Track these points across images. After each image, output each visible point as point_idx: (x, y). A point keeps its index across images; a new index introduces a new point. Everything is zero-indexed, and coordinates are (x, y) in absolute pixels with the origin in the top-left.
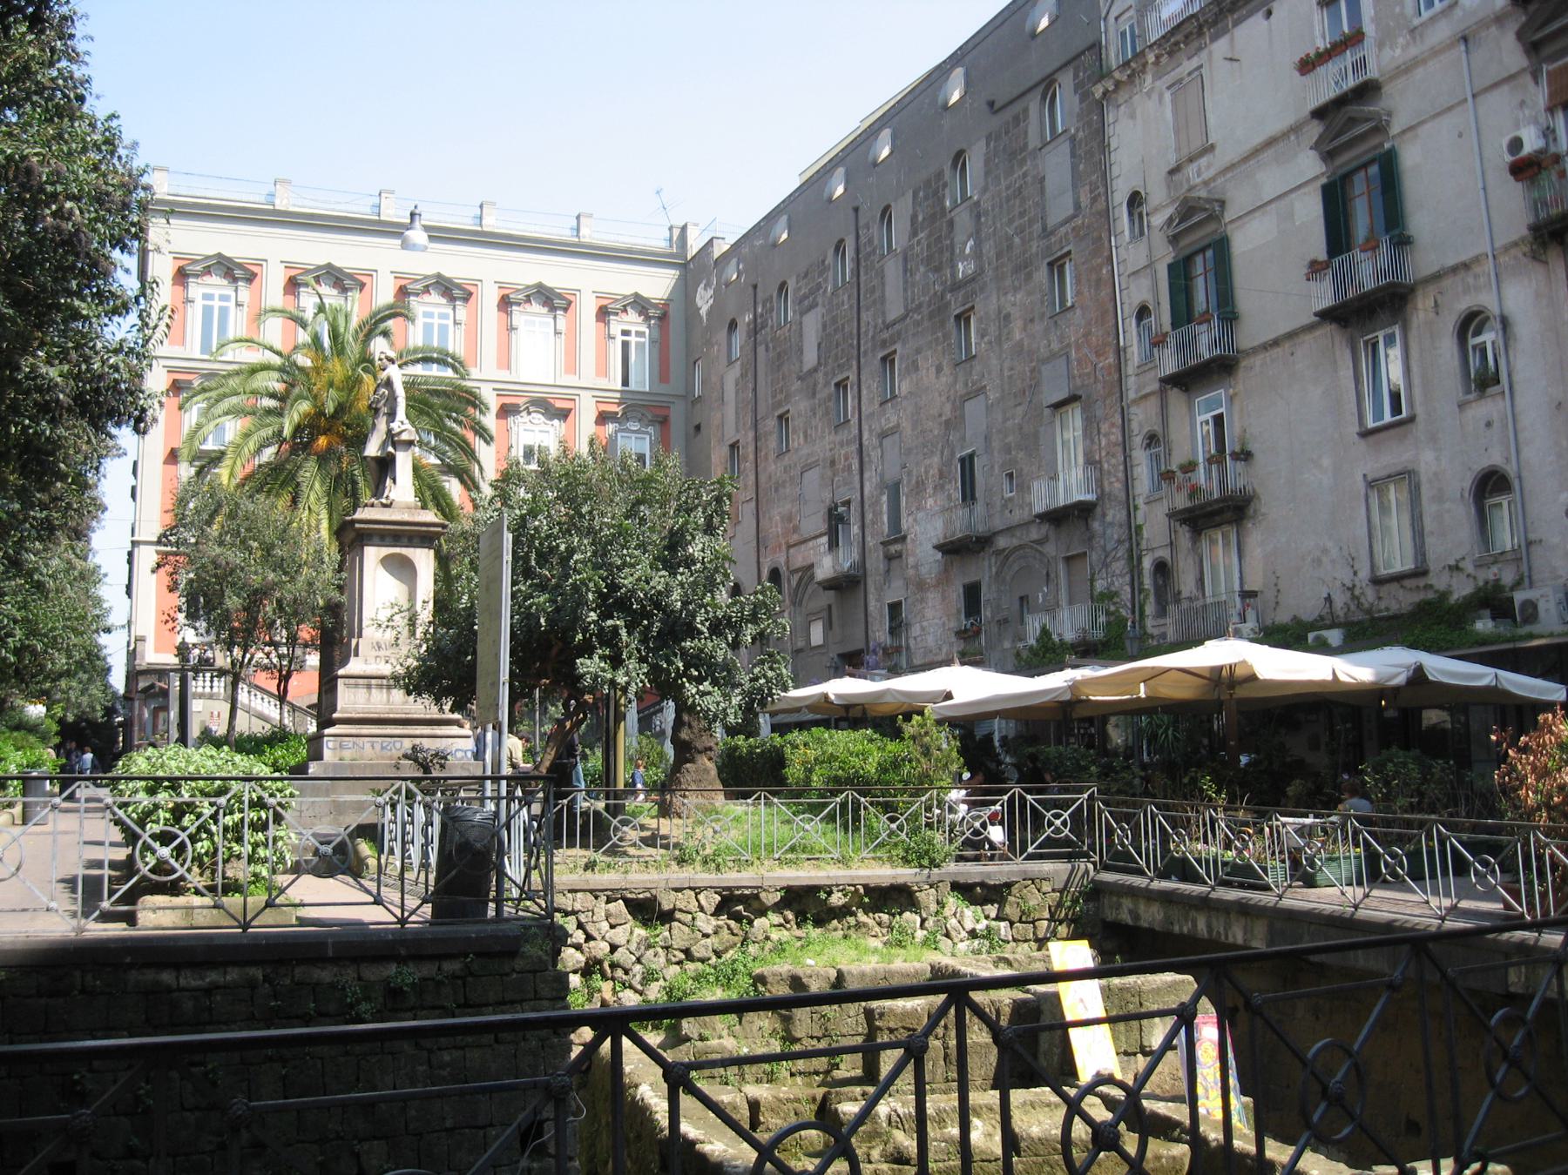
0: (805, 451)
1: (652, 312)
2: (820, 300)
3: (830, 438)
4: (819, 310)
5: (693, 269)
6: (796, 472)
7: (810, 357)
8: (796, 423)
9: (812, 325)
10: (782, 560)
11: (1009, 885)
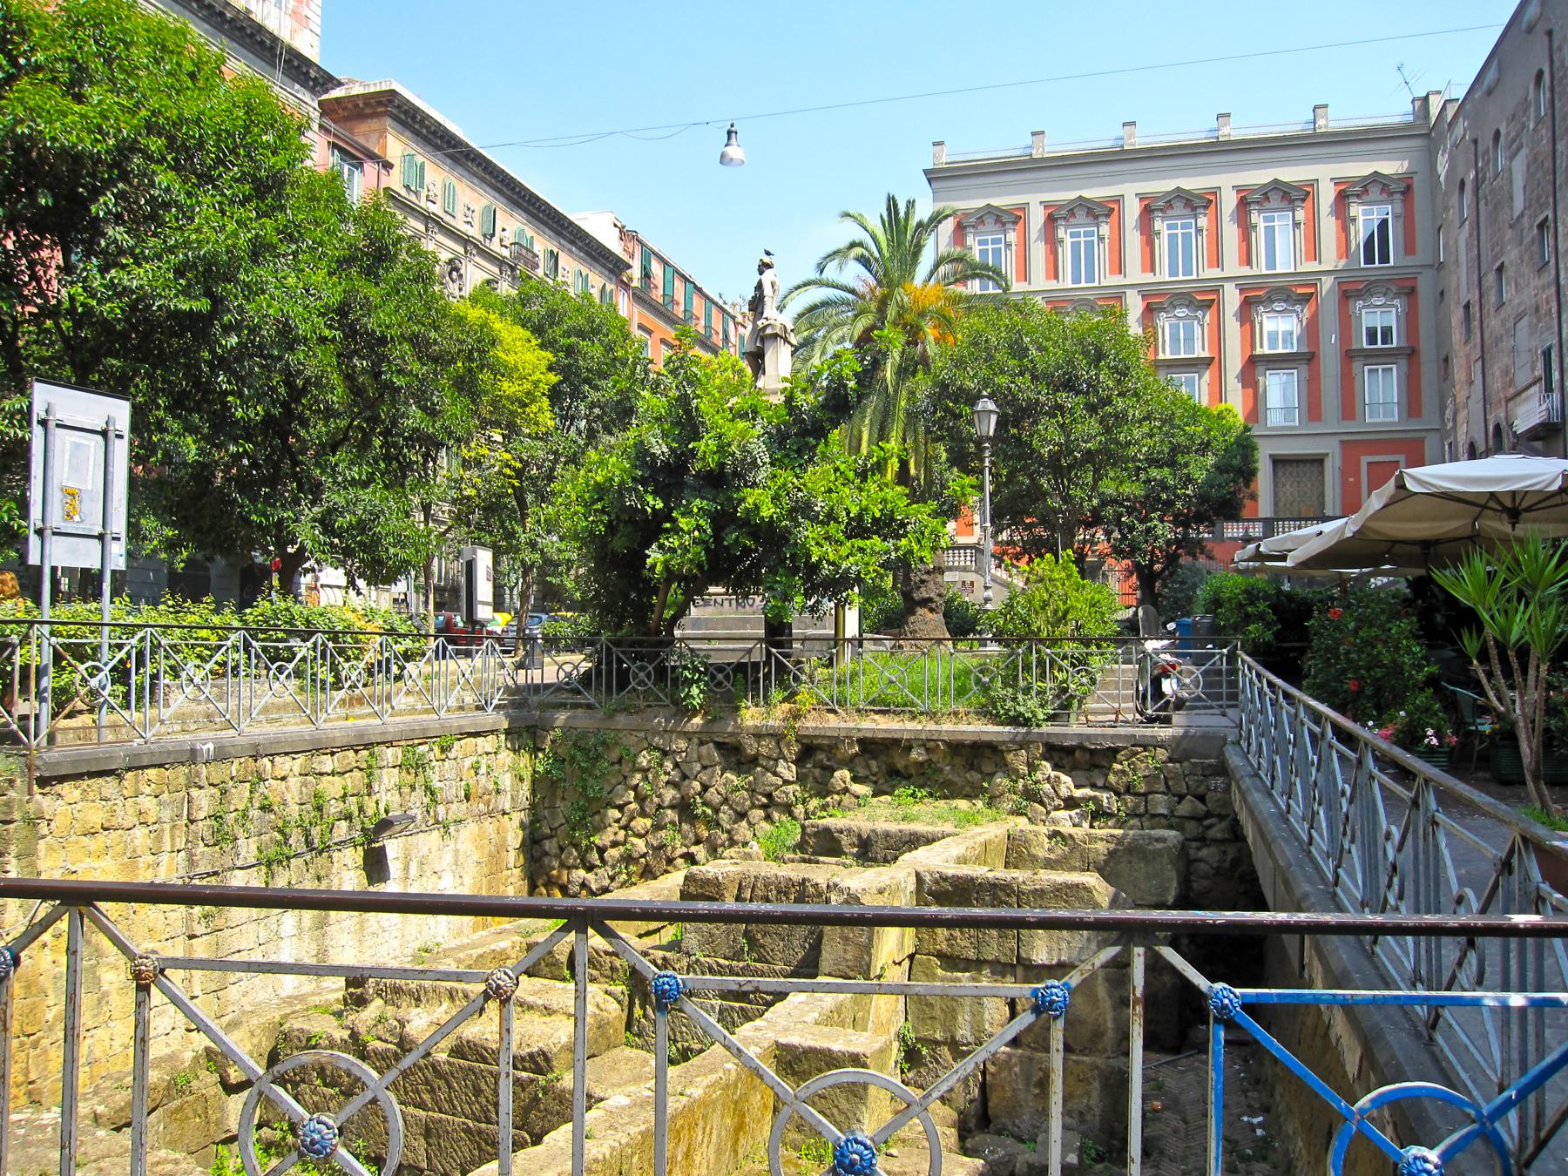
0: (1516, 302)
1: (1393, 187)
2: (1524, 140)
3: (1536, 282)
4: (1524, 151)
5: (1423, 131)
6: (1509, 324)
7: (1519, 203)
8: (1509, 272)
9: (1519, 166)
10: (1502, 415)
11: (1114, 751)
